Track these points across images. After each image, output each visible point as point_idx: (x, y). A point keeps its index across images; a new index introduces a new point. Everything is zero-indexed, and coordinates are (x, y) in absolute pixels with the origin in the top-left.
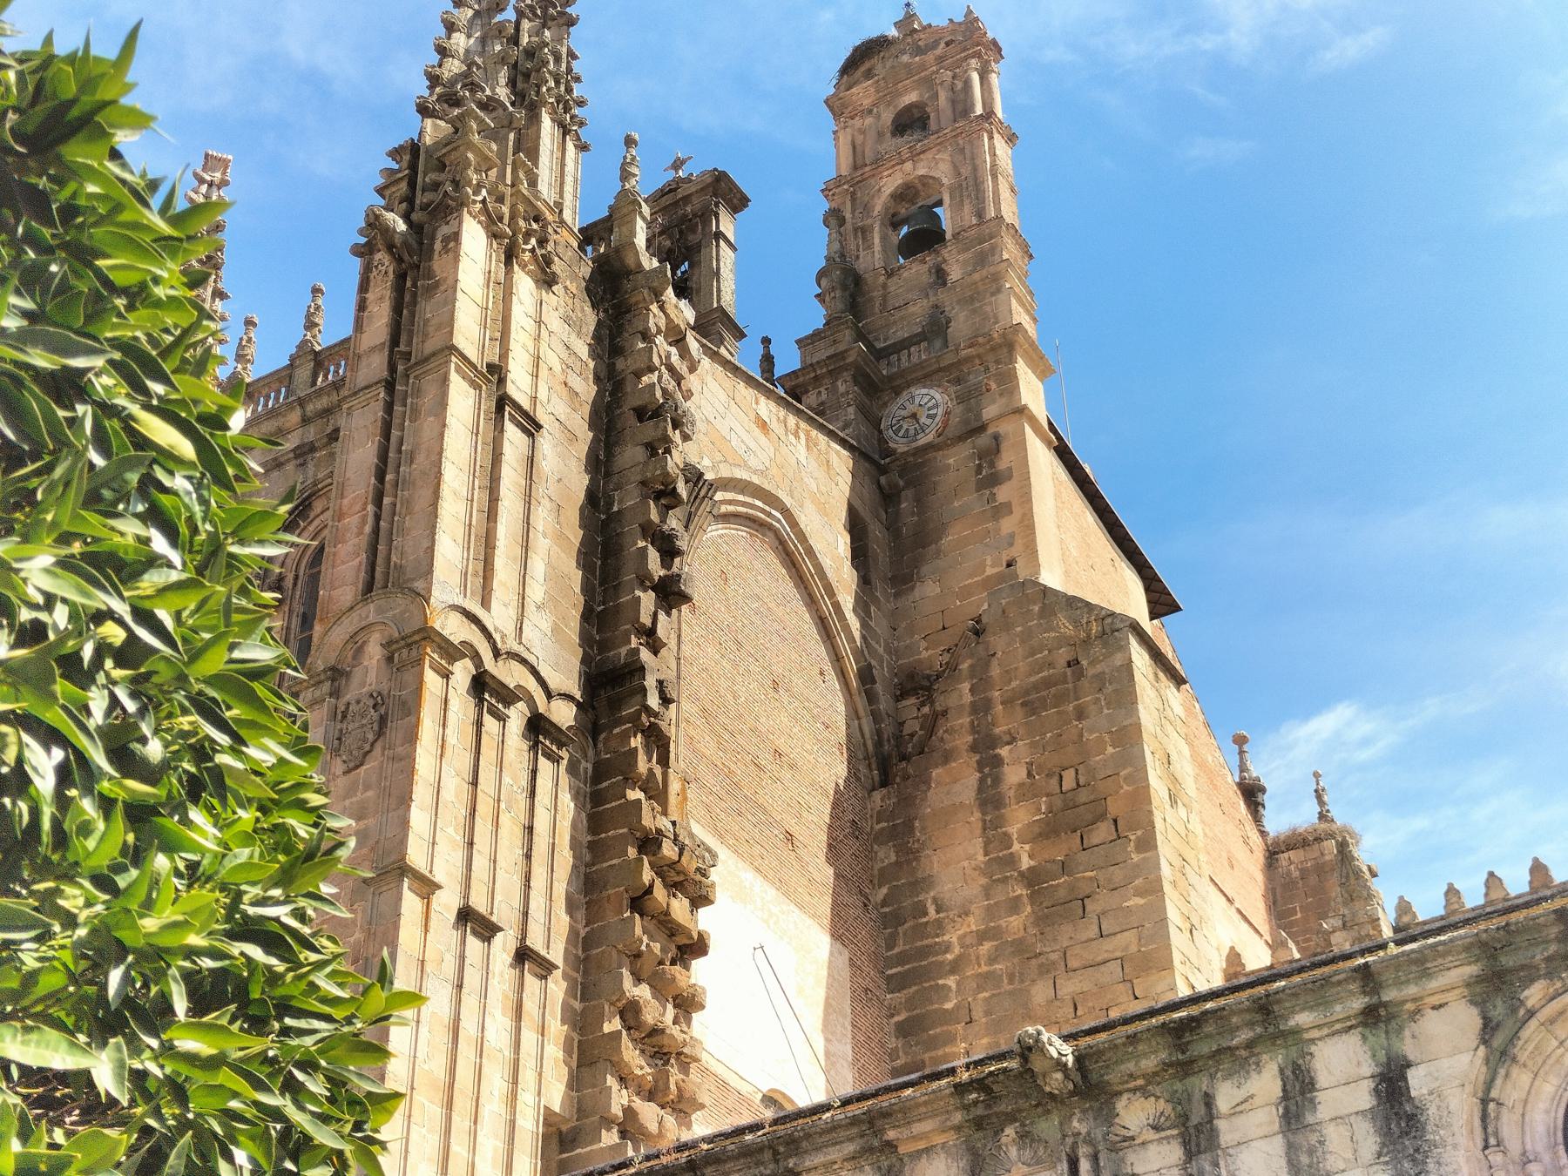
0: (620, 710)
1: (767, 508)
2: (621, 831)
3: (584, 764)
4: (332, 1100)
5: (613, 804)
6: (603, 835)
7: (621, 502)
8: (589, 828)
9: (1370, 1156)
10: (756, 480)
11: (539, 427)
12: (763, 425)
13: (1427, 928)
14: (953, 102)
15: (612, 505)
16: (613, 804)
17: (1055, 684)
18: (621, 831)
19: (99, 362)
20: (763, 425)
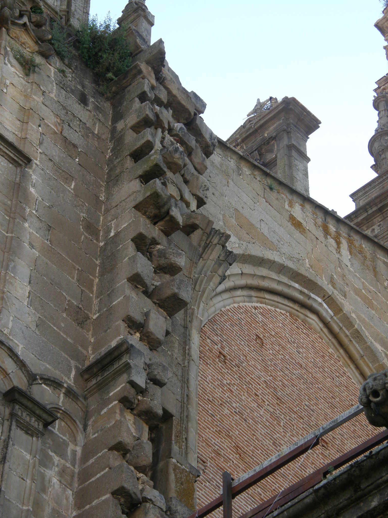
0: (109, 393)
1: (306, 291)
2: (103, 498)
3: (71, 447)
4: (166, 512)
5: (98, 475)
6: (88, 507)
7: (117, 226)
8: (75, 505)
9: (324, 239)
10: (290, 264)
11: (28, 161)
12: (298, 225)
13: (21, 405)
14: (383, 98)
15: (109, 231)
16: (98, 475)
17: (350, 339)
18: (103, 498)
19: (119, 322)
20: (298, 225)
